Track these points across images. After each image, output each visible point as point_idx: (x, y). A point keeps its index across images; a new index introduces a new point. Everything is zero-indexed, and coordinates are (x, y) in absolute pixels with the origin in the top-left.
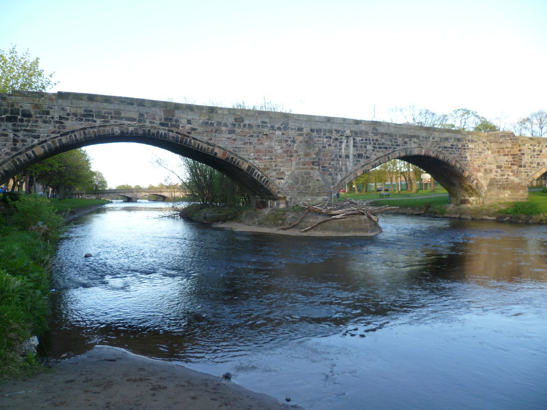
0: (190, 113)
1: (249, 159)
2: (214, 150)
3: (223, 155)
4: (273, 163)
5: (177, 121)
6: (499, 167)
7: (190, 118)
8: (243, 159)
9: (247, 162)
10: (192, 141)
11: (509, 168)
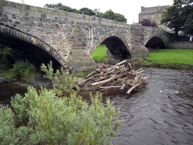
0: (14, 9)
1: (50, 44)
2: (31, 39)
3: (36, 43)
4: (62, 46)
5: (5, 16)
6: (136, 41)
7: (14, 13)
8: (47, 44)
9: (49, 46)
10: (17, 32)
11: (140, 41)
